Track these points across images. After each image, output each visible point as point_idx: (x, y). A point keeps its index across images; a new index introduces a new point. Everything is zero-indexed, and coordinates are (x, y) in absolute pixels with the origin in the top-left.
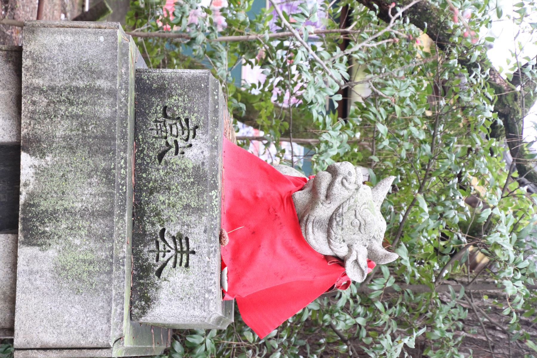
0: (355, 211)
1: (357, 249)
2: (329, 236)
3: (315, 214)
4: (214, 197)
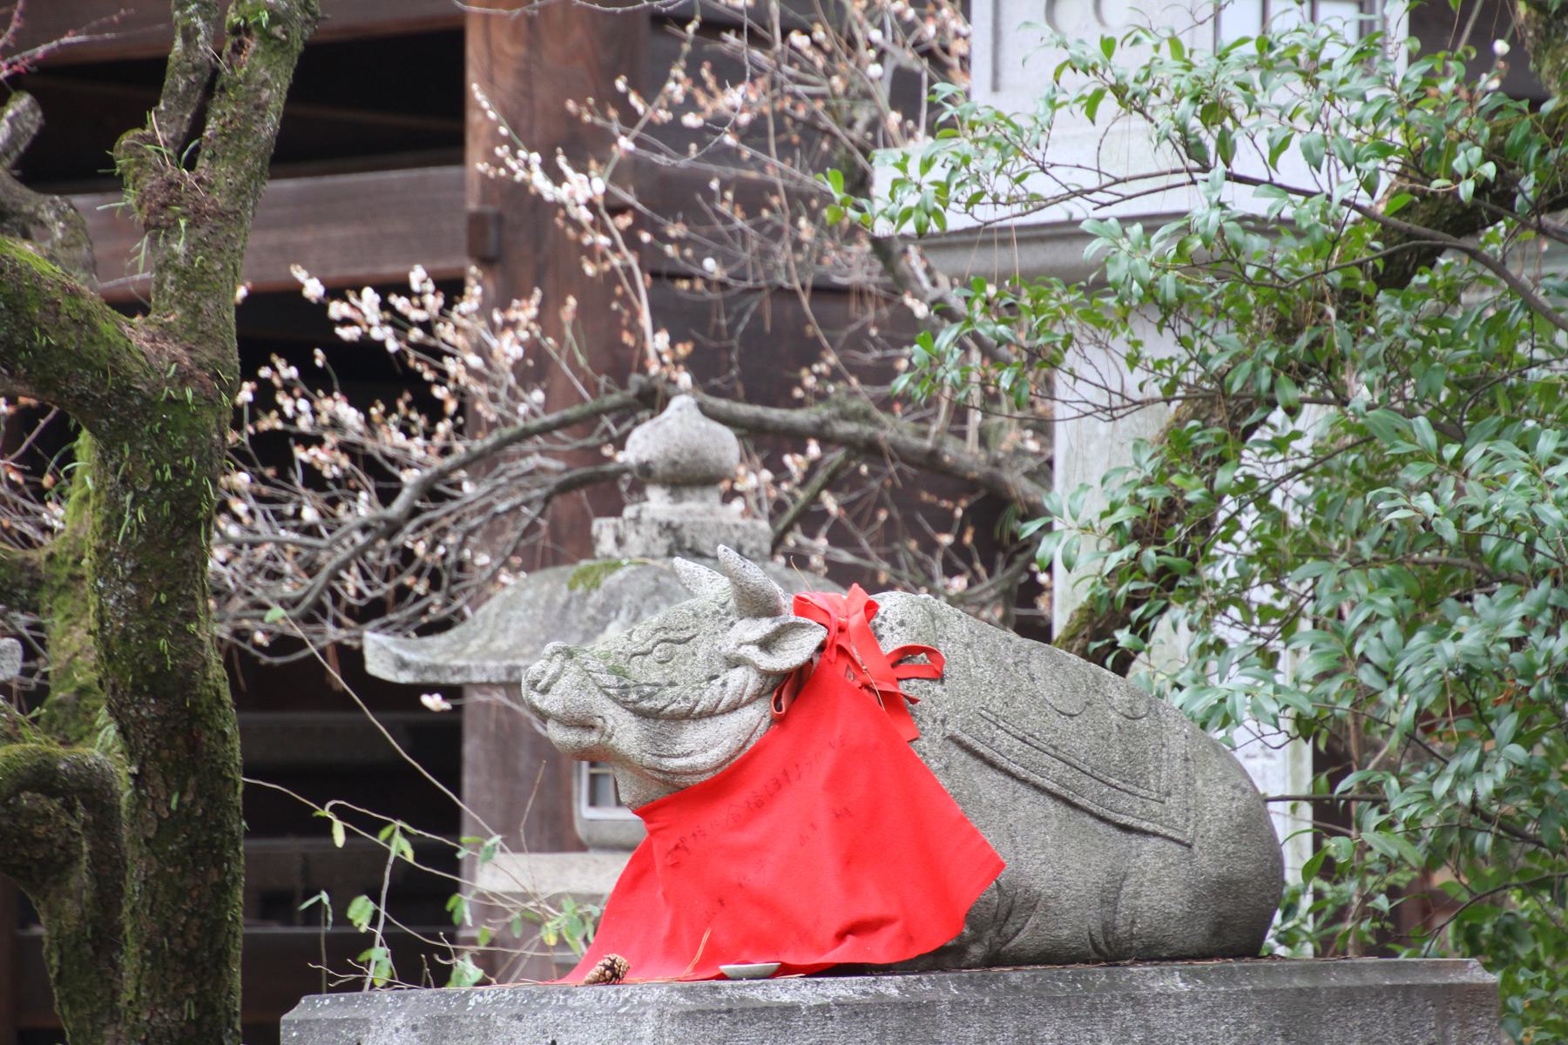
0: (635, 655)
1: (732, 646)
2: (689, 716)
3: (635, 752)
4: (480, 999)
